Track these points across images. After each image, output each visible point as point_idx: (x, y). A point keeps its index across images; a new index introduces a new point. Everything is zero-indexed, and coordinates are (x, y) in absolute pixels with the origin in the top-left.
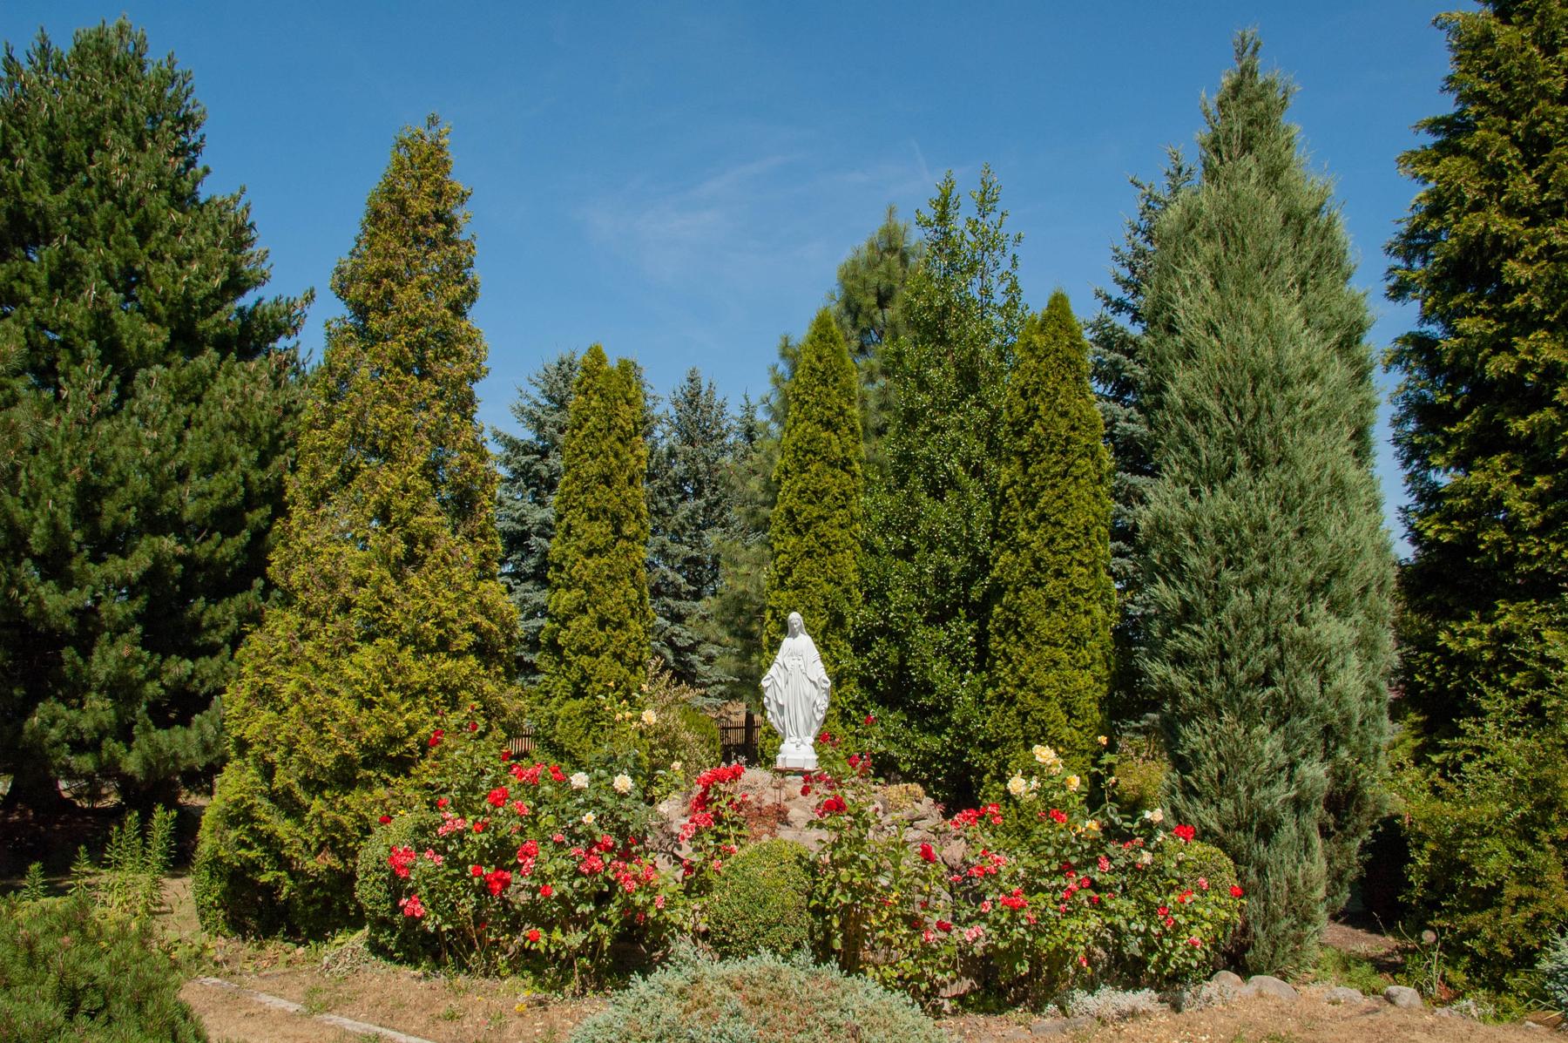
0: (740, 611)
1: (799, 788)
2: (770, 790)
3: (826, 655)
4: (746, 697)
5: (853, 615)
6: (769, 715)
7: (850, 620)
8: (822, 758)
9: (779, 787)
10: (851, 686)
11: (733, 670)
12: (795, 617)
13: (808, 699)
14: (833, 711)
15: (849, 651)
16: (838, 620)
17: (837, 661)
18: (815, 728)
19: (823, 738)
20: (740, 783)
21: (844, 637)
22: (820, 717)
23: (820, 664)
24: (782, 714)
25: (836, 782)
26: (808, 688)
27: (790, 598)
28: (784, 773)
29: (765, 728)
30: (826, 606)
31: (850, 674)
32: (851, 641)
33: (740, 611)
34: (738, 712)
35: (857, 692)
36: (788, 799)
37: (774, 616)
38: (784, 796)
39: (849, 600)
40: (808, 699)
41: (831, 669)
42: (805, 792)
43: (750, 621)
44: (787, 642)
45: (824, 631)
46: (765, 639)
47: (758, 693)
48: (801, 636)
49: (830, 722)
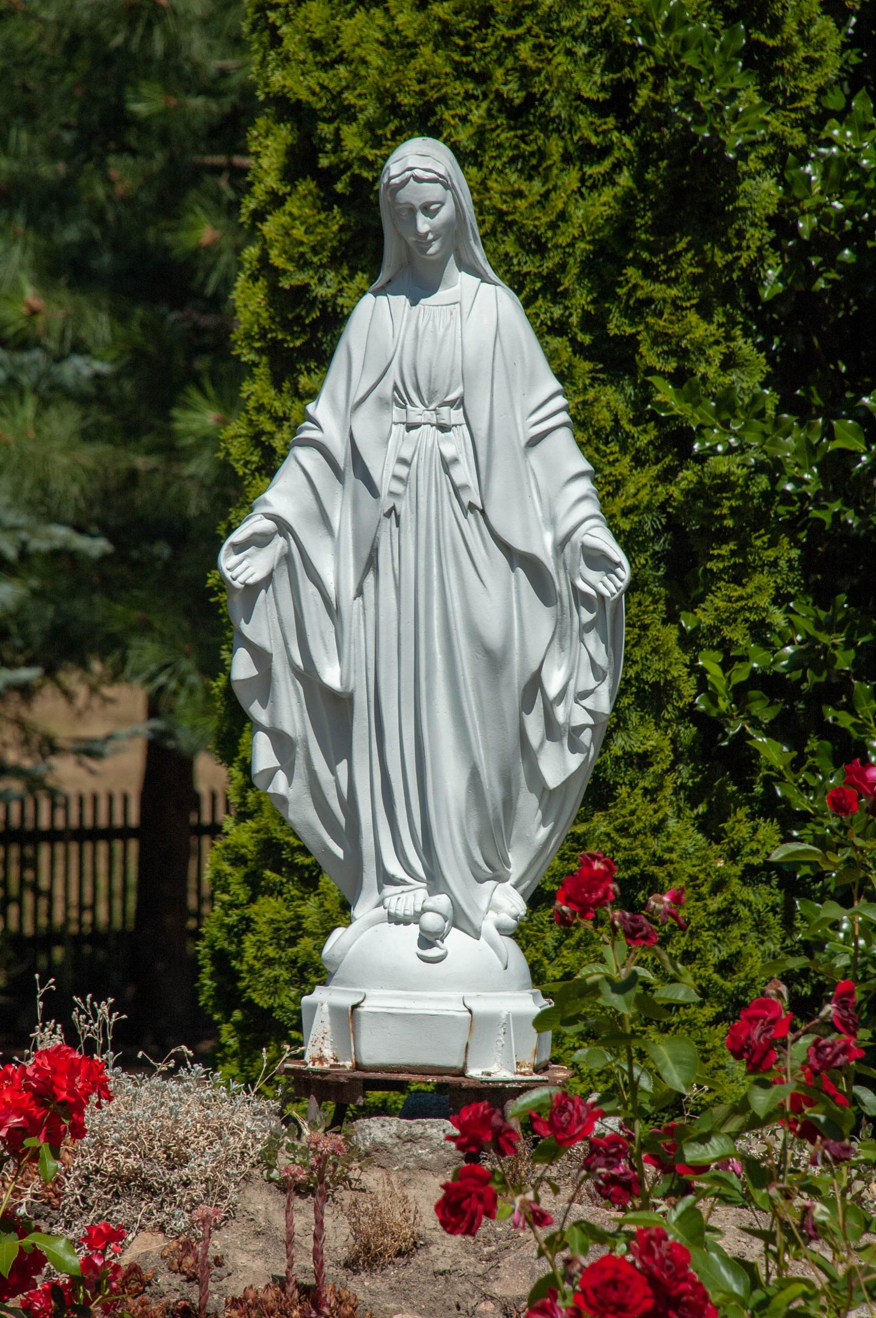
0: (108, 128)
1: (428, 1192)
2: (262, 1202)
3: (612, 401)
4: (146, 652)
5: (782, 159)
6: (264, 755)
7: (763, 192)
8: (568, 1009)
9: (313, 1186)
10: (761, 588)
11: (70, 489)
12: (420, 163)
13: (494, 661)
14: (647, 737)
15: (749, 381)
16: (688, 191)
17: (677, 441)
18: (534, 834)
19: (574, 905)
20: (79, 1156)
21: (728, 291)
22: (559, 765)
23: (566, 455)
24: (339, 747)
25: (650, 1153)
26: (496, 599)
27: (400, 48)
28: (348, 1095)
29: (241, 835)
30: (617, 102)
31: (755, 518)
32: (763, 320)
33: (108, 128)
34: (95, 739)
35: (796, 625)
36: (366, 1258)
37: (300, 163)
38: (339, 1236)
39: (761, 62)
40: (494, 661)
41: (640, 484)
42: (462, 1209)
43: (172, 193)
44: (377, 322)
45: (605, 261)
46: (249, 301)
47: (208, 619)
48: (460, 285)
49: (631, 801)
